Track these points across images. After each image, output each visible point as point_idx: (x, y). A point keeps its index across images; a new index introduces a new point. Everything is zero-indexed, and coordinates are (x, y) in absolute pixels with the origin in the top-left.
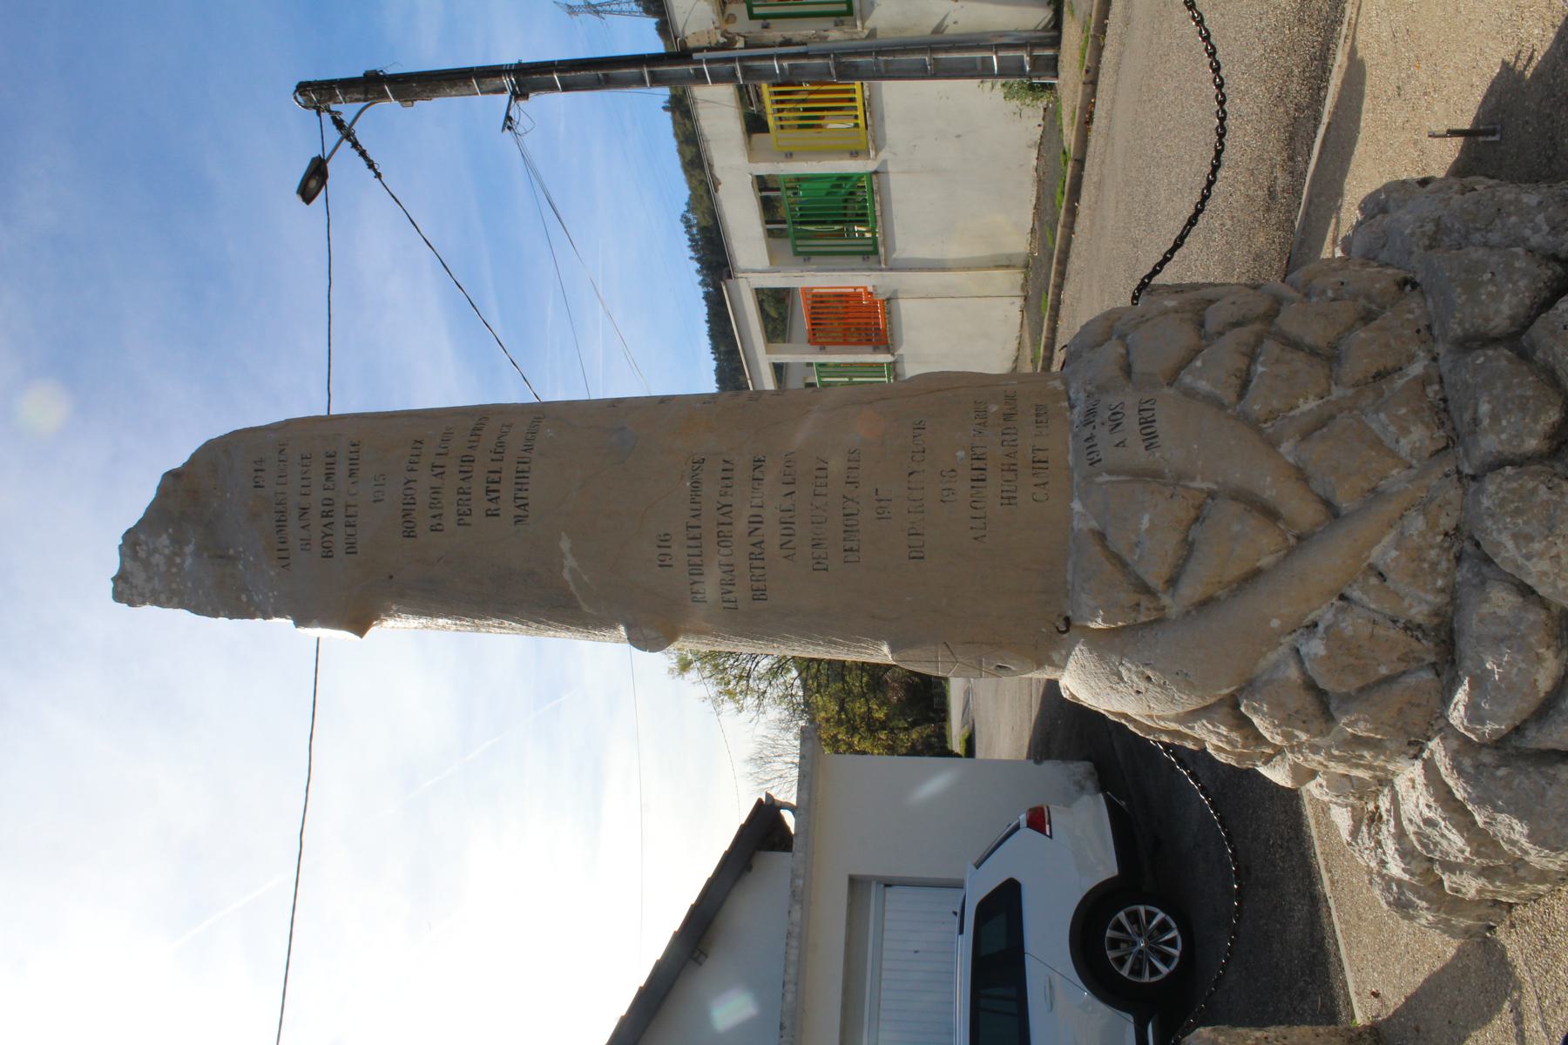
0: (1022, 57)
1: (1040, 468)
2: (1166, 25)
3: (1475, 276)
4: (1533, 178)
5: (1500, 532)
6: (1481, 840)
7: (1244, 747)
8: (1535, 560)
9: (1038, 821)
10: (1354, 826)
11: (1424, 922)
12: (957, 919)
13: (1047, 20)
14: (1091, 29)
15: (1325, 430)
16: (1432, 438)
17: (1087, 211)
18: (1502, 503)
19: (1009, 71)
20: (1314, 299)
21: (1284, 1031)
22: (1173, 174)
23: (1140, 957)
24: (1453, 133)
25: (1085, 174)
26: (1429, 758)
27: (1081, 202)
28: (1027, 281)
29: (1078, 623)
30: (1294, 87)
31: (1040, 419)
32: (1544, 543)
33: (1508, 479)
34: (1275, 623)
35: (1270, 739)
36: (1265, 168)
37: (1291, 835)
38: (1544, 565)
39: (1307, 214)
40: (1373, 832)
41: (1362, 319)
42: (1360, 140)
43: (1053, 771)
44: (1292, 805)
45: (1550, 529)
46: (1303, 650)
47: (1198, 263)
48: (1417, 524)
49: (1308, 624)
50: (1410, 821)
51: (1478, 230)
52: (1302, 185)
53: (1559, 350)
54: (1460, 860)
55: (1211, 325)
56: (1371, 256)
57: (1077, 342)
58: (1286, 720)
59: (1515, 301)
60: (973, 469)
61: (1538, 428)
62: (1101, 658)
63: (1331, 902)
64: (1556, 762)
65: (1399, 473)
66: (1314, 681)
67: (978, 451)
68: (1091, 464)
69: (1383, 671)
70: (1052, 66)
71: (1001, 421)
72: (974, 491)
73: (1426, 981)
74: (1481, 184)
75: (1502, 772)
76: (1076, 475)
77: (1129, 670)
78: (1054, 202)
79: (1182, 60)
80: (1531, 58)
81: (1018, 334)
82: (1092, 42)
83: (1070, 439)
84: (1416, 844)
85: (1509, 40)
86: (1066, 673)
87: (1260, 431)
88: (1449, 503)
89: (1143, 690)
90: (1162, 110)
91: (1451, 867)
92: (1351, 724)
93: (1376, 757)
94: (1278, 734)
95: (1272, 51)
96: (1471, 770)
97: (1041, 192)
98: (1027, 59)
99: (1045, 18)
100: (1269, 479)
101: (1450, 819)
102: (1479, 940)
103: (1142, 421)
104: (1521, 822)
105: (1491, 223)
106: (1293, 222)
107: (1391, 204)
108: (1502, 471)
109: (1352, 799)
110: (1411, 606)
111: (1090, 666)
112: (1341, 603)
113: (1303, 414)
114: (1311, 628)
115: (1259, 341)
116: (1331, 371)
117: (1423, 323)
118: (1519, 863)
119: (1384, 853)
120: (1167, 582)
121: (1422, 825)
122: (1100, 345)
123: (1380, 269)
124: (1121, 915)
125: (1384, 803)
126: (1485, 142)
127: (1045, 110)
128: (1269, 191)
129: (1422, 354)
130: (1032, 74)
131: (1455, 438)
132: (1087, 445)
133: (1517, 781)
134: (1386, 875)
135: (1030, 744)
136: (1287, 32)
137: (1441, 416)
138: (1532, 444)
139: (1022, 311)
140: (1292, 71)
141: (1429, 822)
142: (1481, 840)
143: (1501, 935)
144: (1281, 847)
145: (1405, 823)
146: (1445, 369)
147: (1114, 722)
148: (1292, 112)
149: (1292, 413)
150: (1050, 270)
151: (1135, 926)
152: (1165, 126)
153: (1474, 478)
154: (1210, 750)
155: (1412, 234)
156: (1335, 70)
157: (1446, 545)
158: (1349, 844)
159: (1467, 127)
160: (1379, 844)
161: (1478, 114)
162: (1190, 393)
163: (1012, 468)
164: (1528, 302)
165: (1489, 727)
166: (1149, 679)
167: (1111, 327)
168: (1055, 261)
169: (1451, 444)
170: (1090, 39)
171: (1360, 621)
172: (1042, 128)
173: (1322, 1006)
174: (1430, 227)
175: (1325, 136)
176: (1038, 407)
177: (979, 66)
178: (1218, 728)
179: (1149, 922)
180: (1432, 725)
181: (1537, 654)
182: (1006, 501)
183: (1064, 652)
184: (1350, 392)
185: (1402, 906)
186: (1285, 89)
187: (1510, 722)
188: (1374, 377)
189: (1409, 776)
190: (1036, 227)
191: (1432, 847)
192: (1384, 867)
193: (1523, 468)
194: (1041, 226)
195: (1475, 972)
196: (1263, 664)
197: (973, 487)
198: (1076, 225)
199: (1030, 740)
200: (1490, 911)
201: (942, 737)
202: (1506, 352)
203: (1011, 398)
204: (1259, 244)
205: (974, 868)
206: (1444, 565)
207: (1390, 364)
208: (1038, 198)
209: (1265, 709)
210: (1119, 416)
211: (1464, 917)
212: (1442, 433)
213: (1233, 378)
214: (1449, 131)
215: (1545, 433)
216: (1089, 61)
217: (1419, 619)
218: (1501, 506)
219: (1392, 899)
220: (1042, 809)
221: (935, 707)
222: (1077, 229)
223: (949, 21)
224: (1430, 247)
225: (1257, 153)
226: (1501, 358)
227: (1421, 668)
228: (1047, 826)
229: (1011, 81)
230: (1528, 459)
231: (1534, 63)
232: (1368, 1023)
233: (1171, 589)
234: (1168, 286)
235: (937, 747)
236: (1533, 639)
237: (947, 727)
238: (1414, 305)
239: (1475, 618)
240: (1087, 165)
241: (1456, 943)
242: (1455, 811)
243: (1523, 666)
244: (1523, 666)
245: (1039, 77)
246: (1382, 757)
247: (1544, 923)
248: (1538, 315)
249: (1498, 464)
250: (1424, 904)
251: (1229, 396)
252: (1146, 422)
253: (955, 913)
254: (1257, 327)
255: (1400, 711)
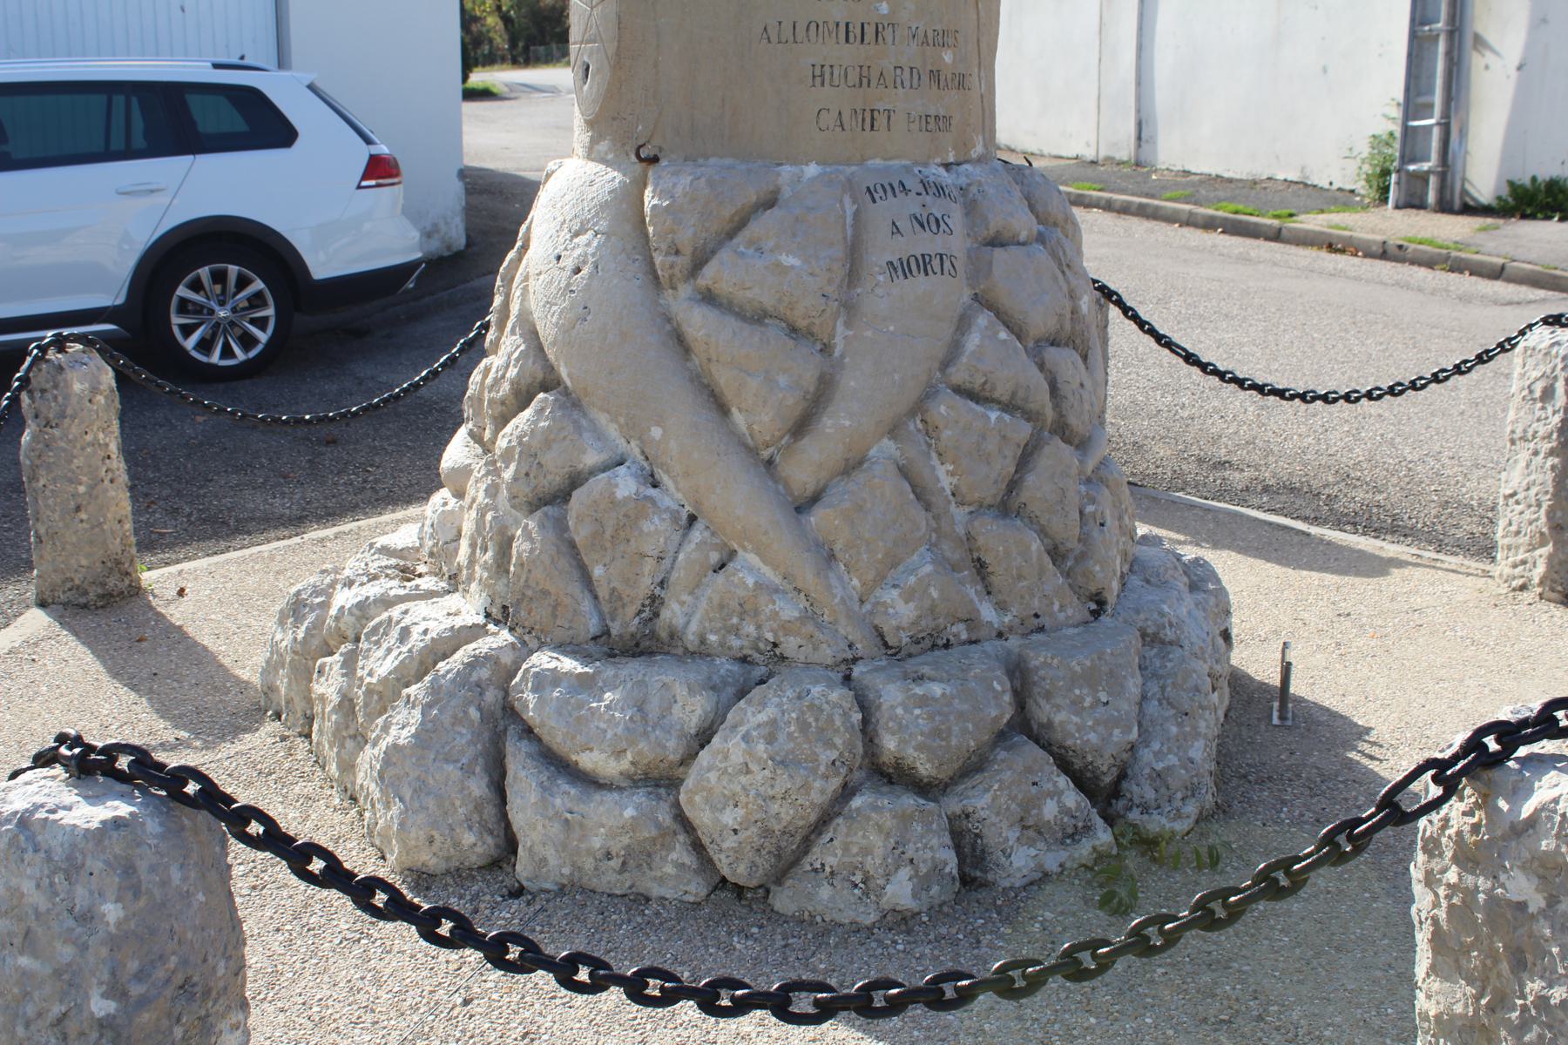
0: (1428, 160)
1: (863, 120)
2: (1454, 345)
3: (1104, 683)
4: (1223, 757)
5: (779, 705)
6: (386, 696)
7: (491, 401)
8: (743, 745)
9: (380, 169)
10: (395, 550)
11: (278, 637)
12: (235, 60)
13: (1476, 195)
14: (1459, 254)
15: (912, 496)
16: (898, 628)
17: (1209, 243)
18: (815, 709)
19: (1411, 140)
20: (1083, 488)
21: (121, 480)
22: (1255, 348)
23: (205, 311)
24: (1286, 670)
25: (1261, 242)
26: (487, 632)
27: (1222, 237)
28: (1118, 164)
29: (650, 174)
30: (1360, 495)
31: (931, 120)
32: (765, 756)
33: (845, 715)
34: (656, 432)
35: (502, 433)
36: (1256, 458)
37: (382, 493)
38: (737, 755)
39: (1193, 506)
40: (389, 572)
41: (1056, 547)
42: (1285, 569)
43: (453, 195)
44: (420, 492)
45: (782, 762)
46: (622, 470)
47: (1133, 376)
48: (789, 610)
49: (657, 476)
50: (406, 612)
51: (1163, 688)
52: (1230, 501)
53: (1007, 776)
54: (360, 673)
55: (1052, 354)
56: (1136, 568)
57: (1037, 179)
58: (529, 452)
59: (1072, 728)
60: (863, 25)
61: (910, 751)
62: (604, 206)
63: (297, 540)
64: (490, 776)
65: (854, 588)
66: (581, 485)
67: (888, 33)
68: (868, 188)
69: (598, 572)
70: (1412, 202)
71: (929, 67)
72: (832, 26)
73: (205, 648)
74: (1219, 700)
75: (474, 714)
76: (854, 168)
77: (588, 245)
78: (1224, 200)
79: (1405, 364)
80: (1372, 758)
81: (1046, 152)
82: (1440, 254)
83: (904, 162)
84: (377, 620)
85: (1397, 735)
86: (582, 162)
87: (912, 413)
88: (815, 649)
89: (562, 264)
90: (1342, 338)
91: (350, 663)
92: (527, 534)
93: (485, 567)
94: (510, 441)
95: (1410, 469)
96: (474, 677)
97: (1240, 185)
98: (1425, 166)
99: (1479, 191)
100: (847, 423)
101: (411, 657)
102: (262, 703)
103: (927, 259)
104: (412, 736)
105: (1169, 704)
106: (1183, 489)
107: (1200, 596)
108: (857, 708)
109: (431, 543)
110: (682, 603)
111: (591, 192)
112: (684, 516)
113: (933, 468)
114: (651, 479)
115: (1029, 416)
116: (990, 506)
117: (1045, 621)
118: (361, 740)
119: (362, 584)
120: (709, 290)
121: (402, 625)
122: (1032, 207)
123: (1119, 574)
124: (258, 285)
125: (427, 583)
126: (1272, 708)
127: (1352, 191)
128: (1226, 462)
129: (1006, 620)
130: (1403, 174)
131: (898, 657)
132: (896, 185)
133: (464, 731)
134: (334, 589)
135: (487, 170)
136: (1433, 488)
137: (927, 641)
138: (890, 744)
139: (1077, 158)
140: (1380, 492)
141: (405, 634)
142: (386, 696)
143: (271, 727)
144: (365, 481)
145: (403, 607)
146: (988, 646)
147: (517, 233)
148: (1327, 491)
149: (934, 455)
150: (1133, 195)
151: (246, 304)
152: (1320, 341)
153: (847, 679)
154: (485, 361)
155: (1162, 614)
156: (1378, 543)
157: (761, 645)
158: (371, 546)
159: (1292, 690)
160: (375, 577)
161: (1307, 701)
162: (963, 324)
163: (863, 81)
164: (1069, 742)
165: (530, 698)
166: (577, 270)
167: (1055, 224)
168: (1144, 200)
169: (890, 652)
170: (1445, 251)
171: (662, 540)
172: (1326, 186)
173: (160, 534)
174: (1169, 634)
175: (1293, 529)
176: (947, 119)
177: (1422, 100)
178: (515, 366)
179: (253, 322)
180: (529, 632)
181: (625, 751)
182: (818, 72)
183: (610, 156)
184: (961, 530)
185: (296, 608)
186: (1359, 483)
187: (538, 721)
188: (979, 559)
189: (467, 608)
190: (1192, 177)
191: (374, 638)
192: (345, 585)
193: (859, 733)
194: (1193, 184)
195: (221, 701)
196: (603, 419)
197: (837, 25)
198: (1192, 229)
199: (492, 171)
200: (299, 715)
201: (491, 60)
202: (1008, 717)
203: (961, 82)
204: (1156, 449)
205: (307, 82)
206: (735, 643)
207: (995, 580)
208: (1230, 181)
209: (542, 424)
210: (934, 228)
211: (290, 684)
212: (905, 640)
213: (983, 380)
214: (1289, 664)
215: (903, 758)
216: (1415, 250)
217: (665, 614)
218: (811, 707)
219: (305, 597)
220: (397, 174)
221: (532, 48)
222: (1186, 231)
223: (1489, 58)
224: (1144, 635)
225: (1276, 449)
226: (1001, 710)
227: (602, 618)
228: (373, 182)
229: (1397, 145)
230: (871, 741)
231: (1365, 761)
232: (144, 584)
233: (699, 297)
234: (1106, 327)
235: (474, 53)
236: (643, 745)
237: (504, 66)
238: (1070, 612)
239: (668, 679)
240: (1273, 244)
241: (256, 680)
242: (421, 663)
243: (609, 735)
244: (609, 735)
245: (1398, 183)
246: (486, 575)
247: (290, 771)
248: (1051, 753)
249: (865, 705)
250: (301, 635)
251: (958, 374)
252: (924, 264)
253: (242, 58)
254: (1050, 414)
255: (546, 593)
